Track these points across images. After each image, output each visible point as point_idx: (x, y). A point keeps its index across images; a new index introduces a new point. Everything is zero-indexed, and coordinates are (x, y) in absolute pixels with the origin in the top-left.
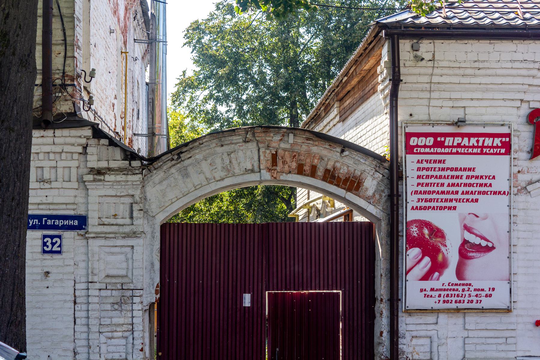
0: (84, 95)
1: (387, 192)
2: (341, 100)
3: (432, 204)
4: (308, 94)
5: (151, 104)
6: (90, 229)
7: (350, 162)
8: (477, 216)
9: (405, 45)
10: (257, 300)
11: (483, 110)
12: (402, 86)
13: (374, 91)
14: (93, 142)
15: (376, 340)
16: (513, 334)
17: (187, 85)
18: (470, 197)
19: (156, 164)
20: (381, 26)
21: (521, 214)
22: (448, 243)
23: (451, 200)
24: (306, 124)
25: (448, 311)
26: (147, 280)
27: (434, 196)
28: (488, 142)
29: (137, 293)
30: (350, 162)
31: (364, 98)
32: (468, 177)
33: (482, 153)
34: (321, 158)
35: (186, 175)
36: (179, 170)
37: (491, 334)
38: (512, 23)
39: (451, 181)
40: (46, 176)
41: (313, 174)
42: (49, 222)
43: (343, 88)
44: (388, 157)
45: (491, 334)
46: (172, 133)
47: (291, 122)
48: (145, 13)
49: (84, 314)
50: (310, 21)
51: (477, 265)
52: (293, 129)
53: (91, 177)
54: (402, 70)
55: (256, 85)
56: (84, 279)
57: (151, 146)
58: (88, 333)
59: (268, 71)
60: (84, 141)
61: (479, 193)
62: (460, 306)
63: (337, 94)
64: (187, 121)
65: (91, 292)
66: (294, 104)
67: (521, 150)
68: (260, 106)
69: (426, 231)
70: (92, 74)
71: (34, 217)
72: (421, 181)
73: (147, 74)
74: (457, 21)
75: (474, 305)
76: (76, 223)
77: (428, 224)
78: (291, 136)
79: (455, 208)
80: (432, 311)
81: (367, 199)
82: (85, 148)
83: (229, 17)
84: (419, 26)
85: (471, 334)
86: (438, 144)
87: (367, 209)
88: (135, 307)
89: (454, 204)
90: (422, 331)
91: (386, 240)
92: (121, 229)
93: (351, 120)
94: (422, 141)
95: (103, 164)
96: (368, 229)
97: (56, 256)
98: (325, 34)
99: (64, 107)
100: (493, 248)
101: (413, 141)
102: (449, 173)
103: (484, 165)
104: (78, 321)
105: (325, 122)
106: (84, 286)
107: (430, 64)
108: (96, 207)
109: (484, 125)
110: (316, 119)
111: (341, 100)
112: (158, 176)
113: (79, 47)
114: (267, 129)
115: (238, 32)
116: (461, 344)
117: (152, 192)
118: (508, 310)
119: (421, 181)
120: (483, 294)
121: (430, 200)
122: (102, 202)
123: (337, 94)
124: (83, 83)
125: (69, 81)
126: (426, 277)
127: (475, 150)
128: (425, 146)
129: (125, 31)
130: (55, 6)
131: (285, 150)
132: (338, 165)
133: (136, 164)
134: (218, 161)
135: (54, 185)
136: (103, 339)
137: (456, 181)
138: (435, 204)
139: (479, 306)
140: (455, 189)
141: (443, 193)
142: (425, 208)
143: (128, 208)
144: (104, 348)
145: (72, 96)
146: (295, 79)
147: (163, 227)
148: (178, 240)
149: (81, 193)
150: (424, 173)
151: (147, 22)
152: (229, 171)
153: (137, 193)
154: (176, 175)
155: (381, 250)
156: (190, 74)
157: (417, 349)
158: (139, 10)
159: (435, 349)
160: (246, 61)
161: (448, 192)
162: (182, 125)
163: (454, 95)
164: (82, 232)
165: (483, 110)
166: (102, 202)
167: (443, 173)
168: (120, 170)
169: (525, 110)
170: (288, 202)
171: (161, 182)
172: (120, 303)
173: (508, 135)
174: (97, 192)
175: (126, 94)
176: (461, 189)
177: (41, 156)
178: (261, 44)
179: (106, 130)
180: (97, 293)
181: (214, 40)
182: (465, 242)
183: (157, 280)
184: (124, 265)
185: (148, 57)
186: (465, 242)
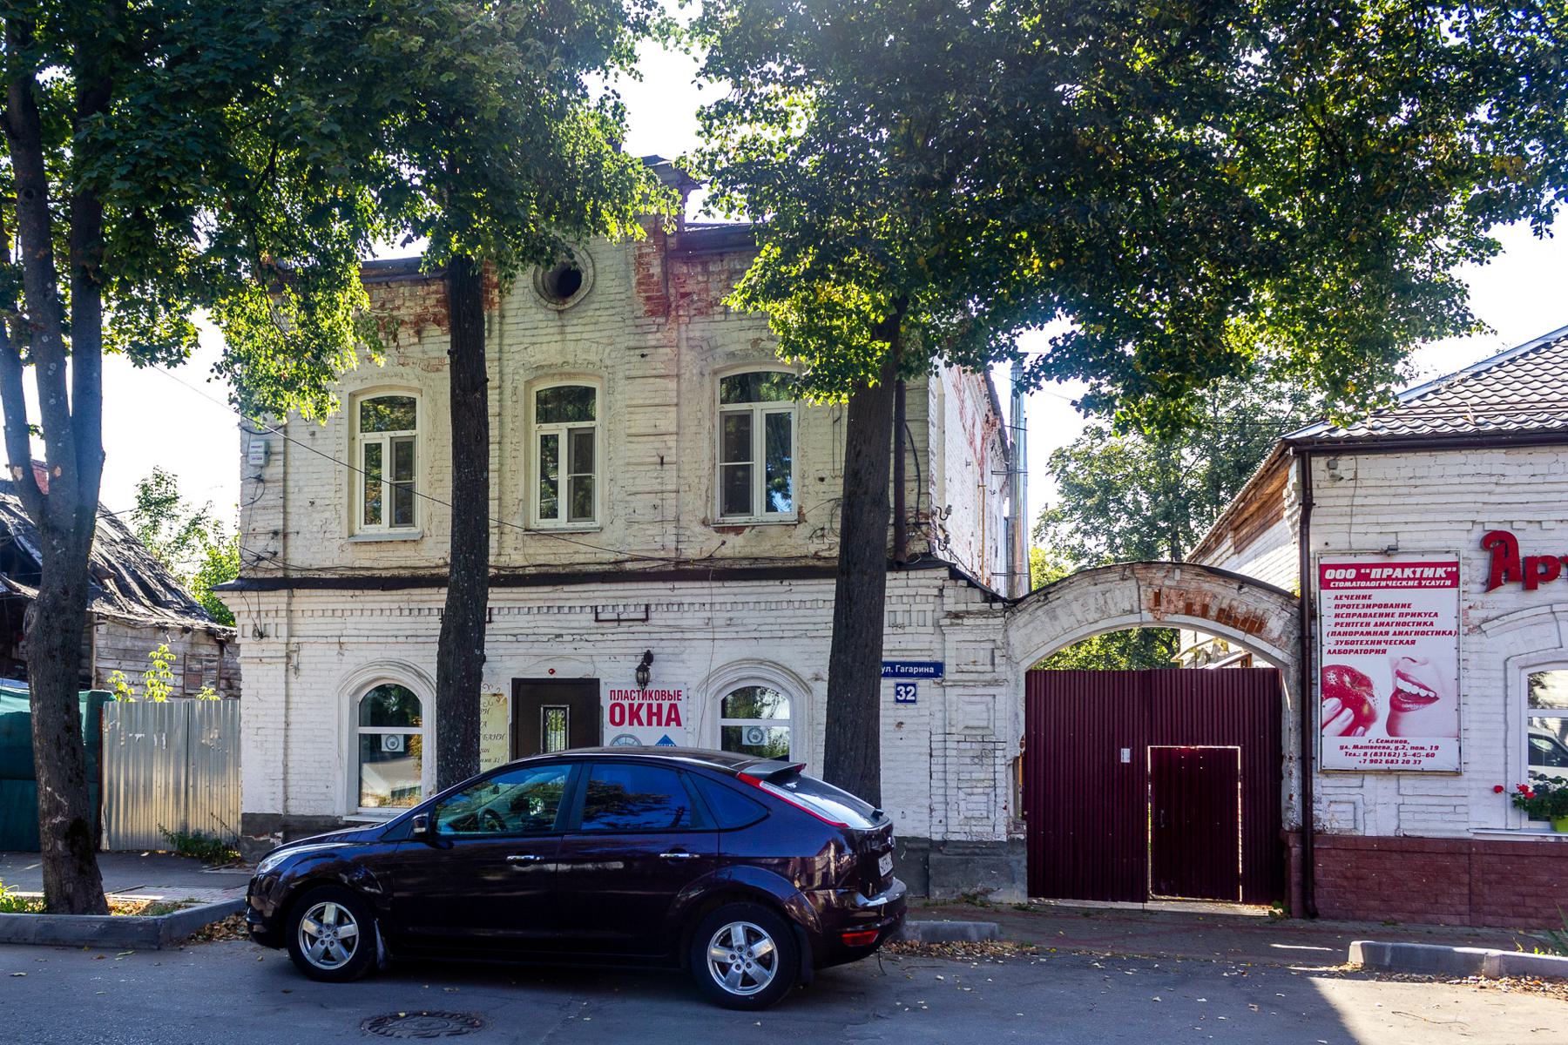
0: (940, 533)
1: (1296, 633)
2: (1236, 529)
3: (1354, 647)
4: (1193, 524)
5: (1011, 540)
8: (628, 378)
9: (1319, 464)
10: (1138, 757)
11: (1422, 536)
12: (1314, 511)
13: (1278, 517)
14: (950, 583)
15: (1284, 804)
16: (1464, 801)
17: (1051, 518)
18: (1405, 638)
19: (1020, 606)
20: (1288, 443)
21: (1473, 657)
22: (1375, 692)
23: (1379, 642)
24: (1191, 558)
25: (1377, 772)
26: (1010, 732)
27: (1358, 638)
28: (1429, 572)
29: (1000, 746)
30: (1250, 600)
31: (1265, 527)
32: (1401, 615)
33: (1420, 586)
35: (1055, 618)
36: (1047, 612)
38: (1460, 430)
40: (899, 621)
41: (1204, 613)
42: (903, 670)
43: (1239, 515)
44: (1298, 593)
46: (1033, 571)
47: (1172, 555)
48: (1003, 442)
49: (941, 768)
51: (1415, 721)
52: (1179, 565)
53: (947, 621)
55: (1131, 516)
57: (1011, 587)
59: (1144, 499)
60: (940, 583)
61: (1417, 633)
62: (1393, 766)
63: (1231, 523)
64: (1048, 558)
65: (948, 744)
67: (1473, 582)
68: (1135, 538)
69: (1347, 679)
70: (948, 511)
71: (887, 664)
72: (1340, 620)
74: (1385, 431)
75: (1411, 766)
76: (932, 670)
77: (1349, 671)
78: (1178, 572)
79: (1384, 651)
80: (1356, 772)
81: (1272, 642)
82: (941, 590)
83: (1098, 441)
84: (1337, 440)
86: (1359, 577)
89: (1383, 646)
92: (982, 677)
93: (1248, 552)
94: (1340, 574)
95: (962, 607)
96: (1272, 677)
97: (910, 706)
98: (1212, 455)
99: (918, 547)
100: (1436, 698)
101: (1330, 574)
102: (1376, 610)
103: (1420, 600)
105: (1216, 555)
106: (941, 738)
107: (1352, 483)
109: (1423, 553)
110: (1205, 550)
111: (1236, 529)
112: (1022, 618)
114: (1149, 565)
115: (1108, 458)
116: (1394, 812)
117: (1016, 636)
118: (1457, 773)
119: (1340, 620)
120: (1424, 753)
121: (1352, 643)
122: (960, 647)
123: (1231, 523)
124: (938, 521)
125: (924, 519)
126: (1348, 732)
127: (1411, 583)
128: (1345, 580)
129: (981, 463)
130: (907, 440)
131: (1170, 588)
132: (1235, 603)
133: (998, 606)
134: (1091, 601)
135: (908, 630)
136: (961, 795)
138: (1359, 647)
139: (1417, 767)
140: (1384, 629)
141: (1368, 633)
142: (1345, 652)
143: (988, 654)
144: (962, 804)
145: (927, 535)
146: (1175, 506)
147: (1029, 674)
148: (1045, 689)
149: (937, 638)
150: (1345, 611)
151: (1005, 452)
152: (1104, 612)
153: (999, 637)
154: (1044, 618)
155: (1288, 700)
156: (1053, 506)
157: (1337, 816)
158: (998, 439)
160: (1118, 489)
161: (1375, 633)
163: (1382, 519)
164: (938, 680)
166: (960, 647)
167: (1368, 611)
168: (980, 613)
169: (1478, 533)
170: (1169, 646)
172: (981, 757)
173: (1456, 564)
174: (954, 636)
176: (1391, 630)
177: (894, 600)
178: (1136, 469)
179: (963, 570)
180: (955, 745)
181: (1082, 468)
182: (1398, 691)
183: (1022, 732)
184: (985, 716)
185: (1007, 489)
186: (1398, 691)
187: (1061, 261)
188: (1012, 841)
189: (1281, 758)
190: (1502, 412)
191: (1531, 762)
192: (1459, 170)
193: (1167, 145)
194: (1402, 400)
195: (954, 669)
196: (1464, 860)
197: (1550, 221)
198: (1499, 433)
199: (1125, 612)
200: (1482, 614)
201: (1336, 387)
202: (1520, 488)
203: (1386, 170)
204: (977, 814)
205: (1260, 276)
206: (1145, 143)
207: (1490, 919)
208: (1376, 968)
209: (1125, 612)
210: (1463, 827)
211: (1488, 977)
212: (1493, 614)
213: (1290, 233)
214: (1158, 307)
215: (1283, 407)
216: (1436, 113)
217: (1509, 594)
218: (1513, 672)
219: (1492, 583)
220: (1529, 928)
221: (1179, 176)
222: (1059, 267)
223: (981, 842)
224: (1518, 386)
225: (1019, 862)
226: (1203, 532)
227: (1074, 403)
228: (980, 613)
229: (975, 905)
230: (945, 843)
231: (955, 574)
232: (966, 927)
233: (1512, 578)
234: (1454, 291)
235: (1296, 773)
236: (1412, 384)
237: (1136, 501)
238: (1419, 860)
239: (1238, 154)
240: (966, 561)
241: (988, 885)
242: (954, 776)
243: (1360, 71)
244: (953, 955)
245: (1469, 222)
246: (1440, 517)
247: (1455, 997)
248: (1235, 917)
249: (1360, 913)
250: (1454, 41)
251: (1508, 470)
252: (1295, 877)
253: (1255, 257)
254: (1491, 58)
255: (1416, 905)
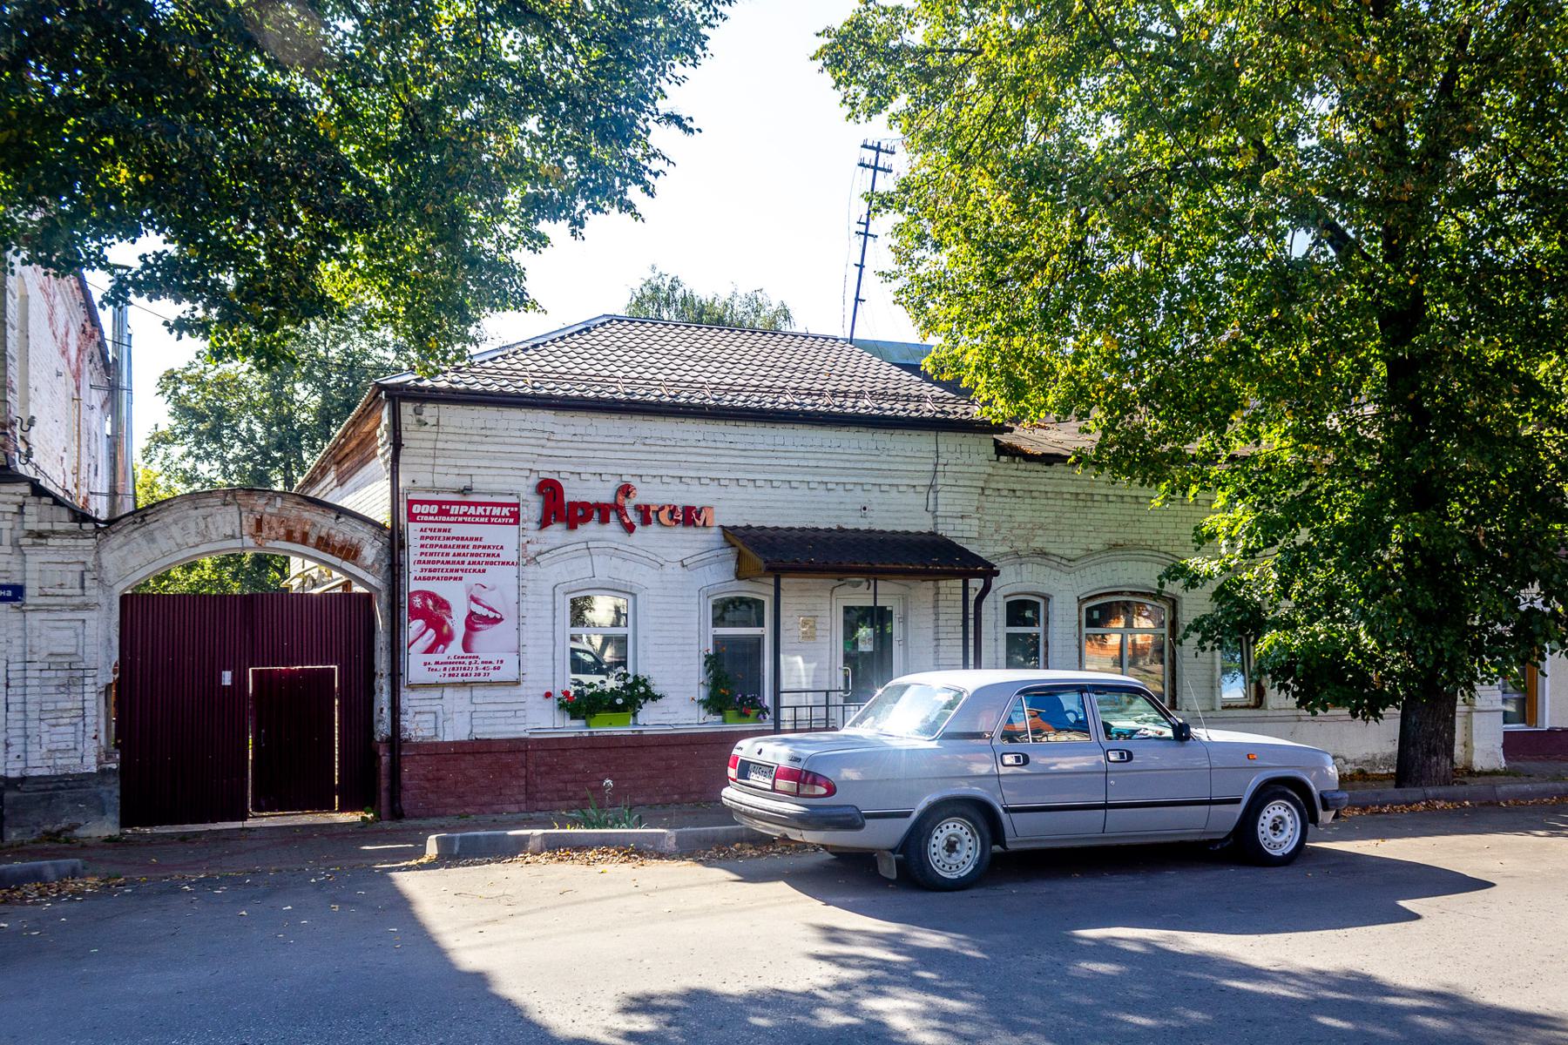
1: (387, 561)
4: (305, 455)
6: (28, 600)
7: (346, 529)
9: (407, 409)
10: (240, 679)
11: (490, 479)
14: (32, 500)
15: (376, 718)
17: (161, 439)
18: (478, 567)
19: (114, 527)
21: (530, 585)
26: (102, 659)
28: (497, 511)
29: (90, 673)
30: (346, 529)
31: (364, 462)
34: (314, 525)
35: (153, 540)
36: (143, 535)
37: (500, 707)
39: (457, 551)
41: (304, 540)
44: (388, 525)
45: (500, 707)
46: (140, 493)
48: (104, 356)
50: (308, 377)
51: (485, 638)
53: (29, 541)
54: (404, 434)
55: (244, 443)
56: (19, 659)
57: (113, 506)
58: (25, 721)
59: (258, 428)
60: (20, 499)
62: (467, 679)
63: (334, 457)
65: (28, 674)
66: (288, 465)
68: (249, 466)
69: (430, 602)
73: (108, 426)
74: (462, 386)
76: (9, 593)
77: (432, 595)
80: (437, 685)
81: (366, 568)
82: (21, 507)
84: (423, 389)
85: (479, 708)
86: (442, 512)
87: (368, 579)
88: (87, 689)
89: (459, 574)
90: (425, 706)
91: (387, 611)
92: (69, 601)
93: (350, 484)
94: (425, 509)
95: (46, 526)
96: (368, 599)
101: (416, 509)
102: (455, 542)
103: (491, 534)
104: (11, 707)
105: (321, 486)
106: (20, 666)
108: (36, 575)
109: (492, 494)
110: (312, 482)
111: (338, 463)
112: (116, 540)
113: (13, 390)
115: (221, 385)
117: (109, 558)
118: (517, 683)
123: (334, 457)
124: (18, 433)
126: (430, 650)
129: (77, 375)
131: (271, 515)
133: (88, 526)
134: (192, 526)
137: (461, 551)
139: (487, 679)
140: (460, 559)
144: (46, 737)
146: (288, 439)
147: (124, 599)
148: (141, 614)
149: (15, 560)
150: (428, 542)
151: (107, 366)
152: (205, 536)
153: (90, 560)
154: (140, 540)
158: (97, 352)
159: (440, 725)
160: (231, 417)
162: (154, 484)
164: (17, 604)
165: (490, 479)
168: (68, 533)
169: (534, 480)
170: (281, 571)
171: (120, 547)
172: (67, 686)
173: (517, 505)
175: (79, 446)
176: (467, 559)
178: (250, 398)
179: (51, 487)
180: (37, 674)
181: (193, 392)
182: (472, 613)
183: (116, 658)
184: (73, 642)
186: (472, 613)
187: (151, 177)
188: (103, 772)
189: (374, 674)
190: (553, 380)
191: (574, 672)
192: (515, 168)
193: (261, 85)
194: (476, 360)
195: (36, 592)
196: (522, 757)
197: (582, 227)
198: (549, 397)
199: (226, 537)
200: (536, 548)
201: (420, 340)
202: (565, 445)
203: (458, 154)
204: (62, 746)
205: (350, 228)
206: (239, 78)
207: (541, 805)
208: (450, 857)
209: (226, 537)
210: (522, 728)
211: (533, 854)
212: (545, 548)
213: (376, 192)
214: (252, 239)
215: (387, 355)
216: (496, 115)
217: (557, 532)
218: (559, 597)
219: (544, 523)
220: (569, 809)
221: (272, 117)
222: (148, 181)
223: (66, 775)
224: (565, 359)
225: (111, 792)
226: (311, 460)
227: (166, 323)
228: (68, 533)
229: (60, 842)
230: (23, 779)
231: (38, 491)
232: (40, 867)
233: (559, 519)
234: (513, 272)
235: (386, 688)
236: (483, 347)
237: (249, 430)
238: (487, 759)
239: (333, 112)
240: (56, 477)
241: (74, 820)
242: (36, 707)
243: (435, 61)
244: (24, 898)
245: (525, 215)
246: (505, 464)
247: (505, 874)
248: (330, 825)
249: (440, 810)
250: (513, 58)
251: (557, 429)
252: (384, 783)
253: (343, 210)
254: (538, 79)
255: (486, 798)
